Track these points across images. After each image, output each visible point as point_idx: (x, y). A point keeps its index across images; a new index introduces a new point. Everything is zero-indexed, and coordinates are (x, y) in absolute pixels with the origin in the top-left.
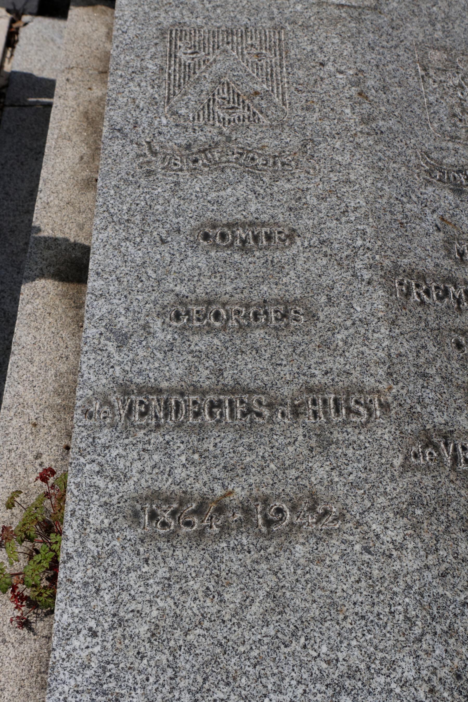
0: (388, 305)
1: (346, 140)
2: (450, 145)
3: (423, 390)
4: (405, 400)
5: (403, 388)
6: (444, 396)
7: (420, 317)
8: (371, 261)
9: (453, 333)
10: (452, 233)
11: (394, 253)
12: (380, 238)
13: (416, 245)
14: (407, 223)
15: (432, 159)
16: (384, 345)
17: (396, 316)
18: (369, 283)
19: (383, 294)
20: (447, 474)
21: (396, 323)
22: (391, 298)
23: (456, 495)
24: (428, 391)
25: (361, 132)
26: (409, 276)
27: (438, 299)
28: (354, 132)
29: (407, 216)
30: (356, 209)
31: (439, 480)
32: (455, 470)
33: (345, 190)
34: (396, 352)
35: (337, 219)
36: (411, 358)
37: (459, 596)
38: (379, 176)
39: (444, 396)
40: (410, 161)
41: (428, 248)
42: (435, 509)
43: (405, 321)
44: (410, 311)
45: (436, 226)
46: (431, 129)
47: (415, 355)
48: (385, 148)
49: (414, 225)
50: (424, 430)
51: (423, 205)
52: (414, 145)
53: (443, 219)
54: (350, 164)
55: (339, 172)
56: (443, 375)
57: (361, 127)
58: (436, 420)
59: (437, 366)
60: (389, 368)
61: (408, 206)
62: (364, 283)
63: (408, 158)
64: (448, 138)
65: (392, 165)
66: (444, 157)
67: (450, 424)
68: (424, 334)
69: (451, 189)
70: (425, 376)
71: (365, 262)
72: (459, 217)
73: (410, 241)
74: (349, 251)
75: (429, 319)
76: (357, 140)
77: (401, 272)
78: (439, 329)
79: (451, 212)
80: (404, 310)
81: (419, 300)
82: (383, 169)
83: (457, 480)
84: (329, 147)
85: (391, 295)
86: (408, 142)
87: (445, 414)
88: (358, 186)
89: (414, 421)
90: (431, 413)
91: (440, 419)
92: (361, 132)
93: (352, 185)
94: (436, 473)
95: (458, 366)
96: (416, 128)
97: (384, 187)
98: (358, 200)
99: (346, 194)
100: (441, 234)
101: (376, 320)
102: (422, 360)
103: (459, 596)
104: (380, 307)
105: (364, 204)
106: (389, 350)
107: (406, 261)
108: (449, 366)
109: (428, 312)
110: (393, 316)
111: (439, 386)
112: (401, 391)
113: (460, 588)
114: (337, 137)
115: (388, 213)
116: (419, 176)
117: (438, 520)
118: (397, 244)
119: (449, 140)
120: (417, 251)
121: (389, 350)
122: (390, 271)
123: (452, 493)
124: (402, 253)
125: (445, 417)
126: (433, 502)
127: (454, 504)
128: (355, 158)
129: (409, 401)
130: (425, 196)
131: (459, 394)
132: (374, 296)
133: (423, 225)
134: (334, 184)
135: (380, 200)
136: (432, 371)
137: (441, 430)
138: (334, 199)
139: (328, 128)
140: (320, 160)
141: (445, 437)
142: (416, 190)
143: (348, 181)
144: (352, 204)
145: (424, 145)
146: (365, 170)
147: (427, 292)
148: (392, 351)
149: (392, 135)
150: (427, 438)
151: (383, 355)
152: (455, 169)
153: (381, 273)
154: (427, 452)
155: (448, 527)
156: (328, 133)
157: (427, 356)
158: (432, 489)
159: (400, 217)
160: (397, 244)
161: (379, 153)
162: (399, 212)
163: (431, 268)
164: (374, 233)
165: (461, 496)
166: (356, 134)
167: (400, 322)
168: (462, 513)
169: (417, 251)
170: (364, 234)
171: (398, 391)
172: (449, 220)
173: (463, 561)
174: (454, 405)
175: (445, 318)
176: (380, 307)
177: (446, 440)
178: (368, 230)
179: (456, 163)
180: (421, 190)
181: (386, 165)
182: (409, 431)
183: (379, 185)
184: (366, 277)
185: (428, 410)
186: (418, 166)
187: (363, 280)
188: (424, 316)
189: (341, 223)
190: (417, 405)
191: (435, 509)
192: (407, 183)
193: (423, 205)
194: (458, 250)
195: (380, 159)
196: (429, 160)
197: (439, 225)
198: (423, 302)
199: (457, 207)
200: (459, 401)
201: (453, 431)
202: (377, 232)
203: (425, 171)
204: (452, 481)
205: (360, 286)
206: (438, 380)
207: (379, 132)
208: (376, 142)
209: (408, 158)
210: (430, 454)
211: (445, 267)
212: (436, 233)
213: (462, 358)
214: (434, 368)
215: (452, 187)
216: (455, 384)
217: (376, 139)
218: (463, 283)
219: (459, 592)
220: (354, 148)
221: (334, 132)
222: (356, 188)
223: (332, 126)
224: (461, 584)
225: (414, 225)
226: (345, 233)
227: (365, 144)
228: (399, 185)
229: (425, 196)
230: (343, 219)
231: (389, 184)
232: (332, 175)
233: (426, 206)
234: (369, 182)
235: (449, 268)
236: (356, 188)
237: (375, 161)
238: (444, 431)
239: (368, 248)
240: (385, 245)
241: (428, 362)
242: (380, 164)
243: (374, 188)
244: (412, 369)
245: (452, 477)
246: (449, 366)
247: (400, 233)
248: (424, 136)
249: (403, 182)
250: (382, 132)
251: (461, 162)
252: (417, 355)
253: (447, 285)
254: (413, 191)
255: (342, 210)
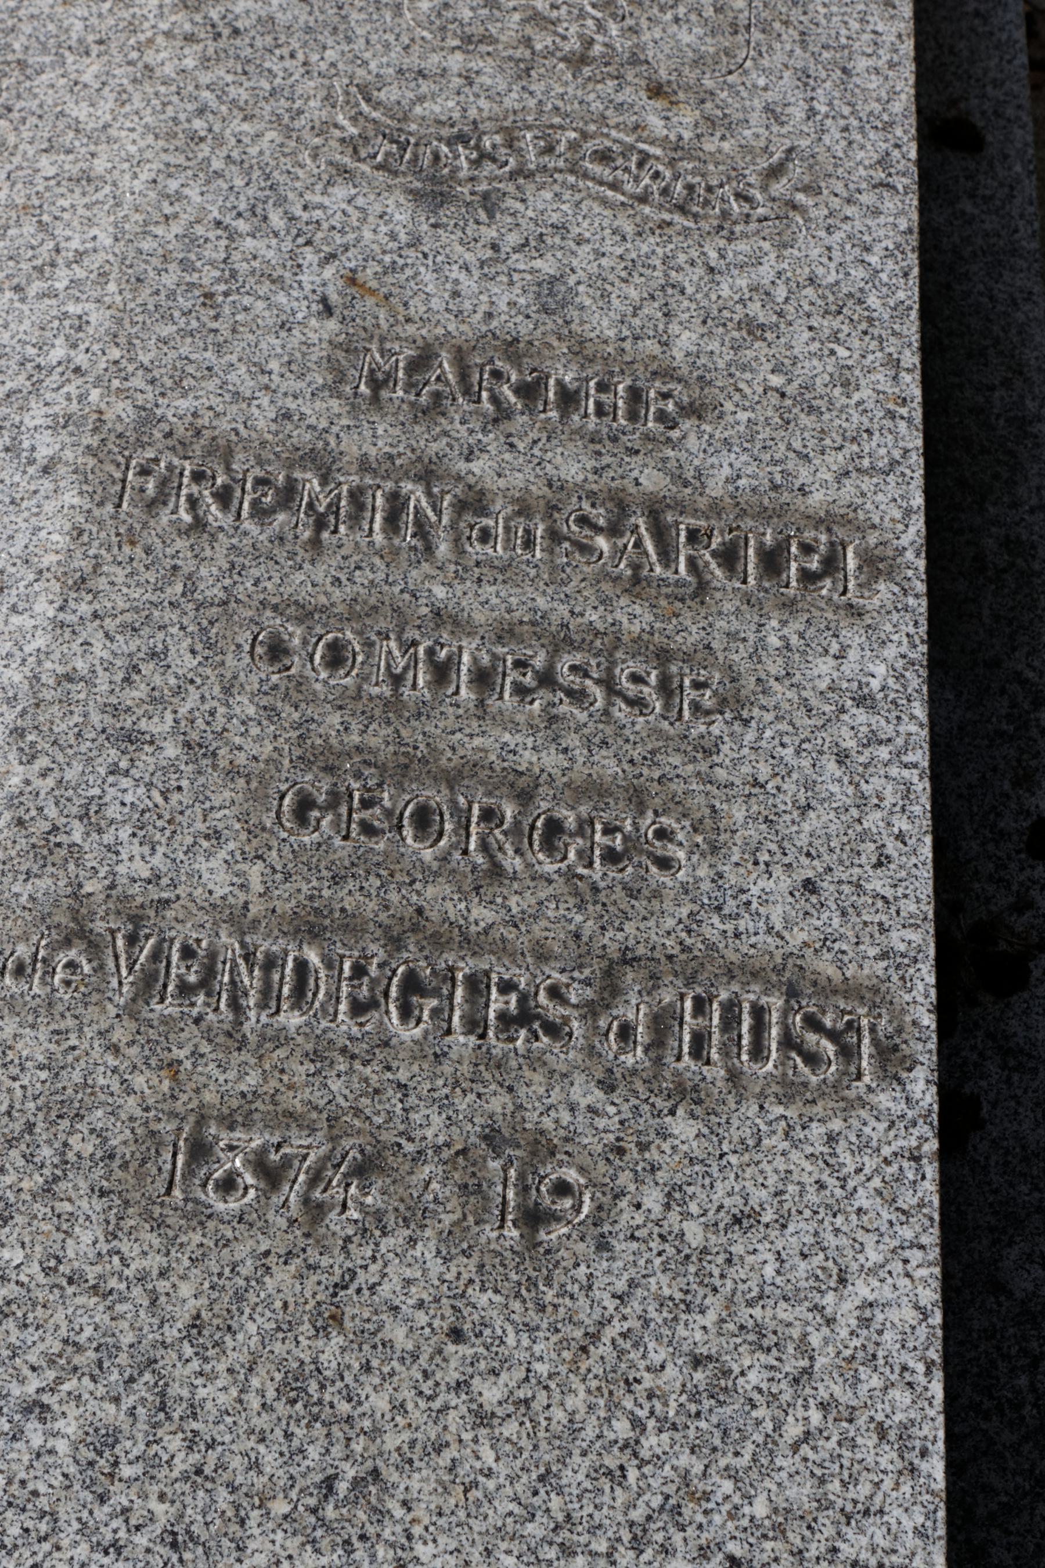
0: (81, 532)
1: (119, 58)
2: (456, 61)
3: (111, 779)
4: (40, 809)
5: (44, 774)
6: (175, 797)
7: (175, 568)
8: (74, 406)
9: (269, 613)
10: (369, 322)
11: (152, 382)
12: (122, 340)
13: (234, 358)
14: (226, 294)
15: (377, 105)
16: (28, 649)
17: (96, 567)
18: (46, 470)
19: (76, 501)
20: (104, 1026)
21: (90, 584)
22: (96, 512)
23: (116, 1087)
24: (125, 783)
25: (168, 34)
26: (183, 448)
27: (252, 516)
28: (149, 34)
29: (234, 273)
30: (80, 256)
31: (73, 1041)
32: (134, 1016)
33: (66, 204)
34: (60, 670)
35: (17, 289)
36: (105, 687)
37: (22, 1381)
38: (181, 160)
39: (175, 797)
40: (300, 112)
41: (274, 365)
42: (30, 1127)
43: (120, 580)
44: (148, 551)
45: (324, 300)
46: (408, 15)
47: (119, 677)
48: (229, 78)
49: (247, 301)
50: (75, 895)
51: (301, 241)
52: (333, 65)
53: (352, 281)
54: (106, 127)
55: (69, 152)
56: (194, 736)
57: (173, 18)
58: (121, 869)
59: (183, 711)
60: (23, 713)
61: (249, 243)
62: (31, 470)
63: (298, 104)
64: (456, 43)
65: (238, 125)
66: (421, 99)
67: (165, 881)
68: (170, 616)
69: (411, 191)
70: (131, 739)
71: (57, 409)
72: (409, 272)
73: (219, 348)
74: (22, 378)
75: (204, 572)
76: (150, 57)
77: (158, 435)
78: (225, 603)
79: (387, 259)
80: (127, 549)
81: (187, 518)
82: (202, 139)
83: (131, 1043)
84: (63, 81)
85: (101, 504)
86: (314, 57)
87: (161, 850)
88: (107, 189)
89: (50, 869)
90: (113, 849)
91: (135, 864)
92: (168, 34)
93: (90, 189)
94: (70, 1022)
95: (251, 711)
96: (355, 16)
97: (186, 191)
98: (95, 231)
99: (66, 216)
100: (332, 325)
101: (32, 577)
102: (140, 692)
103: (22, 1381)
104: (55, 537)
105: (108, 242)
106: (39, 663)
107: (184, 404)
108: (221, 710)
109: (208, 553)
110: (87, 566)
111: (174, 766)
112: (38, 783)
113: (32, 1358)
114: (95, 49)
115: (173, 267)
116: (315, 157)
117: (28, 1158)
118: (173, 354)
119: (454, 49)
120: (232, 377)
121: (39, 663)
122: (120, 436)
123: (101, 1081)
124: (178, 384)
125: (157, 860)
126: (31, 1105)
127: (100, 1113)
128: (128, 108)
129: (52, 812)
130: (318, 214)
131: (227, 794)
132: (49, 507)
133: (281, 298)
134: (41, 188)
135: (159, 231)
136: (160, 725)
137: (127, 898)
138: (29, 228)
139: (79, 25)
140: (24, 120)
141: (136, 920)
142: (291, 196)
143: (86, 178)
144: (75, 244)
145: (366, 63)
146: (142, 144)
147: (224, 497)
148: (48, 665)
149: (269, 39)
150: (74, 919)
151: (17, 678)
152: (445, 132)
153: (88, 440)
154: (62, 958)
155: (56, 1179)
156: (73, 43)
157: (157, 681)
158: (41, 1067)
159: (208, 275)
160: (173, 354)
161: (206, 94)
162: (212, 263)
163: (261, 424)
164: (107, 324)
165: (130, 1091)
166: (150, 41)
167: (102, 583)
168: (114, 1142)
169: (232, 377)
170: (80, 329)
171: (27, 782)
172: (373, 284)
173: (71, 1281)
174: (200, 826)
175: (255, 572)
176: (55, 537)
177: (137, 927)
178: (93, 319)
179: (456, 115)
180: (308, 196)
181: (216, 128)
182: (23, 900)
183: (173, 185)
184: (43, 453)
185: (108, 838)
186: (322, 129)
187: (31, 462)
188: (188, 566)
189: (23, 300)
190: (76, 824)
191: (30, 1127)
192: (268, 177)
193: (301, 241)
194: (372, 371)
195: (201, 112)
196: (364, 107)
197: (334, 298)
198: (199, 524)
199: (415, 242)
200: (219, 815)
201: (167, 901)
202: (119, 322)
203: (343, 140)
204: (115, 1049)
205: (17, 478)
206: (171, 750)
207: (226, 32)
208: (205, 62)
209: (298, 104)
210: (72, 966)
211: (312, 421)
212: (313, 322)
213: (275, 687)
214: (169, 717)
215: (418, 185)
216: (223, 763)
217: (211, 51)
218: (354, 468)
219: (26, 1371)
220: (135, 81)
221: (91, 38)
222: (100, 196)
223: (94, 20)
224: (41, 1347)
225: (247, 301)
226: (26, 325)
227: (169, 69)
228: (239, 182)
229: (318, 214)
230: (37, 286)
231: (208, 182)
232: (44, 161)
233: (309, 243)
234: (145, 176)
235: (324, 424)
236: (100, 196)
237: (182, 117)
238: (139, 900)
239: (77, 370)
240: (130, 360)
241: (155, 699)
242: (198, 124)
243: (152, 194)
244: (95, 718)
245: (118, 1035)
246: (221, 710)
247: (194, 324)
248: (374, 38)
249: (256, 174)
250: (236, 32)
251: (473, 113)
252: (127, 680)
253: (298, 475)
254: (281, 201)
255: (38, 262)
